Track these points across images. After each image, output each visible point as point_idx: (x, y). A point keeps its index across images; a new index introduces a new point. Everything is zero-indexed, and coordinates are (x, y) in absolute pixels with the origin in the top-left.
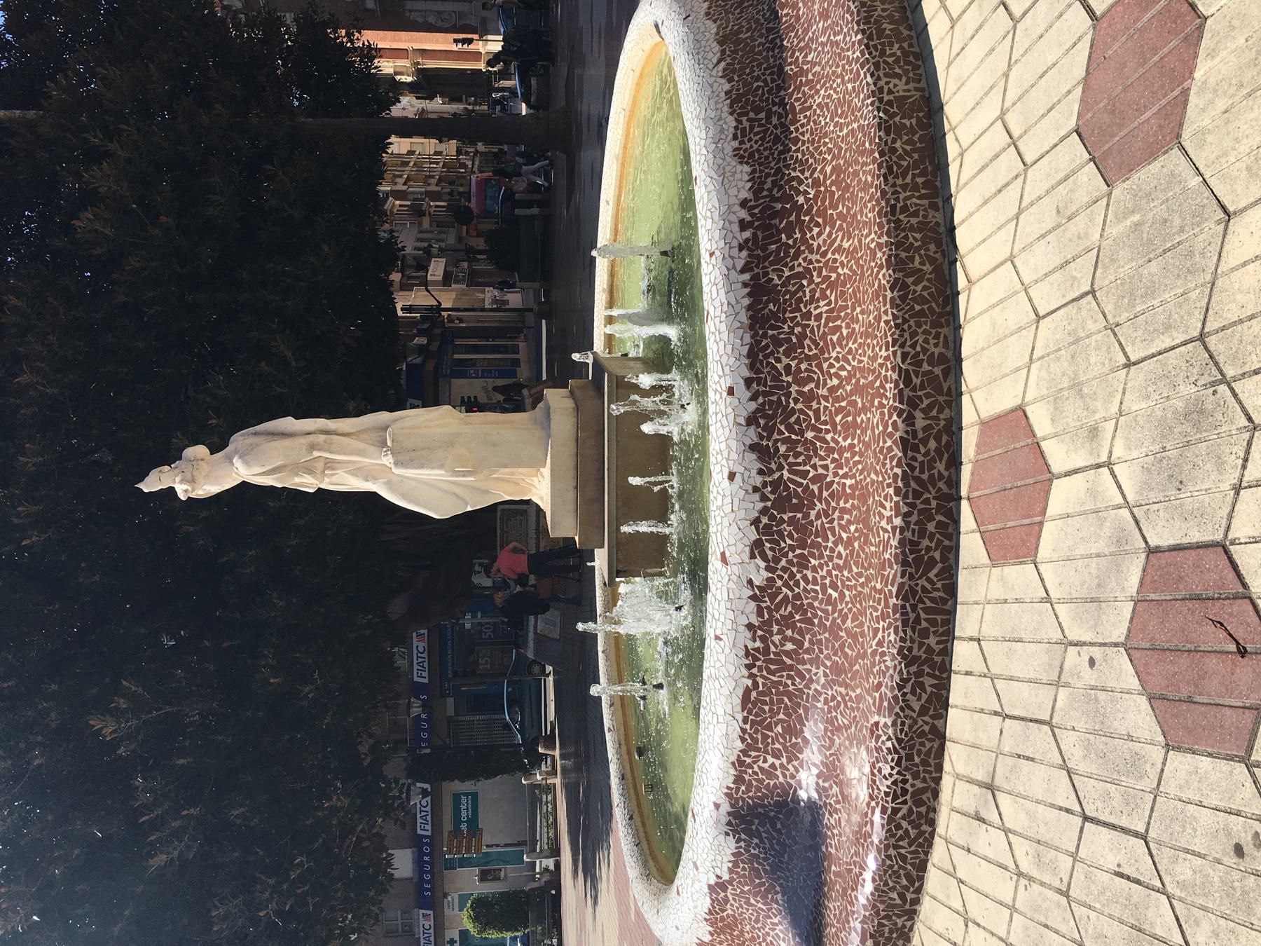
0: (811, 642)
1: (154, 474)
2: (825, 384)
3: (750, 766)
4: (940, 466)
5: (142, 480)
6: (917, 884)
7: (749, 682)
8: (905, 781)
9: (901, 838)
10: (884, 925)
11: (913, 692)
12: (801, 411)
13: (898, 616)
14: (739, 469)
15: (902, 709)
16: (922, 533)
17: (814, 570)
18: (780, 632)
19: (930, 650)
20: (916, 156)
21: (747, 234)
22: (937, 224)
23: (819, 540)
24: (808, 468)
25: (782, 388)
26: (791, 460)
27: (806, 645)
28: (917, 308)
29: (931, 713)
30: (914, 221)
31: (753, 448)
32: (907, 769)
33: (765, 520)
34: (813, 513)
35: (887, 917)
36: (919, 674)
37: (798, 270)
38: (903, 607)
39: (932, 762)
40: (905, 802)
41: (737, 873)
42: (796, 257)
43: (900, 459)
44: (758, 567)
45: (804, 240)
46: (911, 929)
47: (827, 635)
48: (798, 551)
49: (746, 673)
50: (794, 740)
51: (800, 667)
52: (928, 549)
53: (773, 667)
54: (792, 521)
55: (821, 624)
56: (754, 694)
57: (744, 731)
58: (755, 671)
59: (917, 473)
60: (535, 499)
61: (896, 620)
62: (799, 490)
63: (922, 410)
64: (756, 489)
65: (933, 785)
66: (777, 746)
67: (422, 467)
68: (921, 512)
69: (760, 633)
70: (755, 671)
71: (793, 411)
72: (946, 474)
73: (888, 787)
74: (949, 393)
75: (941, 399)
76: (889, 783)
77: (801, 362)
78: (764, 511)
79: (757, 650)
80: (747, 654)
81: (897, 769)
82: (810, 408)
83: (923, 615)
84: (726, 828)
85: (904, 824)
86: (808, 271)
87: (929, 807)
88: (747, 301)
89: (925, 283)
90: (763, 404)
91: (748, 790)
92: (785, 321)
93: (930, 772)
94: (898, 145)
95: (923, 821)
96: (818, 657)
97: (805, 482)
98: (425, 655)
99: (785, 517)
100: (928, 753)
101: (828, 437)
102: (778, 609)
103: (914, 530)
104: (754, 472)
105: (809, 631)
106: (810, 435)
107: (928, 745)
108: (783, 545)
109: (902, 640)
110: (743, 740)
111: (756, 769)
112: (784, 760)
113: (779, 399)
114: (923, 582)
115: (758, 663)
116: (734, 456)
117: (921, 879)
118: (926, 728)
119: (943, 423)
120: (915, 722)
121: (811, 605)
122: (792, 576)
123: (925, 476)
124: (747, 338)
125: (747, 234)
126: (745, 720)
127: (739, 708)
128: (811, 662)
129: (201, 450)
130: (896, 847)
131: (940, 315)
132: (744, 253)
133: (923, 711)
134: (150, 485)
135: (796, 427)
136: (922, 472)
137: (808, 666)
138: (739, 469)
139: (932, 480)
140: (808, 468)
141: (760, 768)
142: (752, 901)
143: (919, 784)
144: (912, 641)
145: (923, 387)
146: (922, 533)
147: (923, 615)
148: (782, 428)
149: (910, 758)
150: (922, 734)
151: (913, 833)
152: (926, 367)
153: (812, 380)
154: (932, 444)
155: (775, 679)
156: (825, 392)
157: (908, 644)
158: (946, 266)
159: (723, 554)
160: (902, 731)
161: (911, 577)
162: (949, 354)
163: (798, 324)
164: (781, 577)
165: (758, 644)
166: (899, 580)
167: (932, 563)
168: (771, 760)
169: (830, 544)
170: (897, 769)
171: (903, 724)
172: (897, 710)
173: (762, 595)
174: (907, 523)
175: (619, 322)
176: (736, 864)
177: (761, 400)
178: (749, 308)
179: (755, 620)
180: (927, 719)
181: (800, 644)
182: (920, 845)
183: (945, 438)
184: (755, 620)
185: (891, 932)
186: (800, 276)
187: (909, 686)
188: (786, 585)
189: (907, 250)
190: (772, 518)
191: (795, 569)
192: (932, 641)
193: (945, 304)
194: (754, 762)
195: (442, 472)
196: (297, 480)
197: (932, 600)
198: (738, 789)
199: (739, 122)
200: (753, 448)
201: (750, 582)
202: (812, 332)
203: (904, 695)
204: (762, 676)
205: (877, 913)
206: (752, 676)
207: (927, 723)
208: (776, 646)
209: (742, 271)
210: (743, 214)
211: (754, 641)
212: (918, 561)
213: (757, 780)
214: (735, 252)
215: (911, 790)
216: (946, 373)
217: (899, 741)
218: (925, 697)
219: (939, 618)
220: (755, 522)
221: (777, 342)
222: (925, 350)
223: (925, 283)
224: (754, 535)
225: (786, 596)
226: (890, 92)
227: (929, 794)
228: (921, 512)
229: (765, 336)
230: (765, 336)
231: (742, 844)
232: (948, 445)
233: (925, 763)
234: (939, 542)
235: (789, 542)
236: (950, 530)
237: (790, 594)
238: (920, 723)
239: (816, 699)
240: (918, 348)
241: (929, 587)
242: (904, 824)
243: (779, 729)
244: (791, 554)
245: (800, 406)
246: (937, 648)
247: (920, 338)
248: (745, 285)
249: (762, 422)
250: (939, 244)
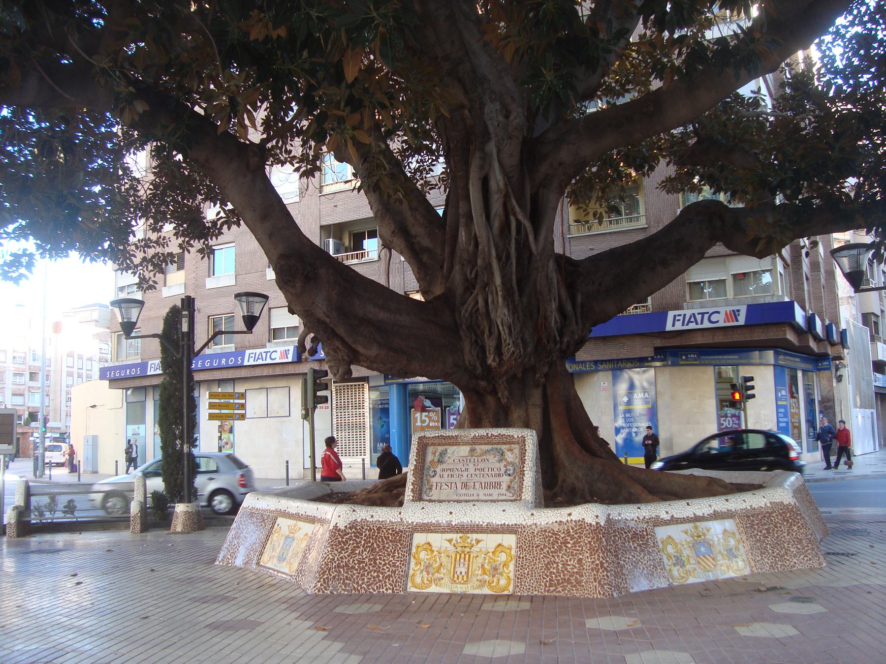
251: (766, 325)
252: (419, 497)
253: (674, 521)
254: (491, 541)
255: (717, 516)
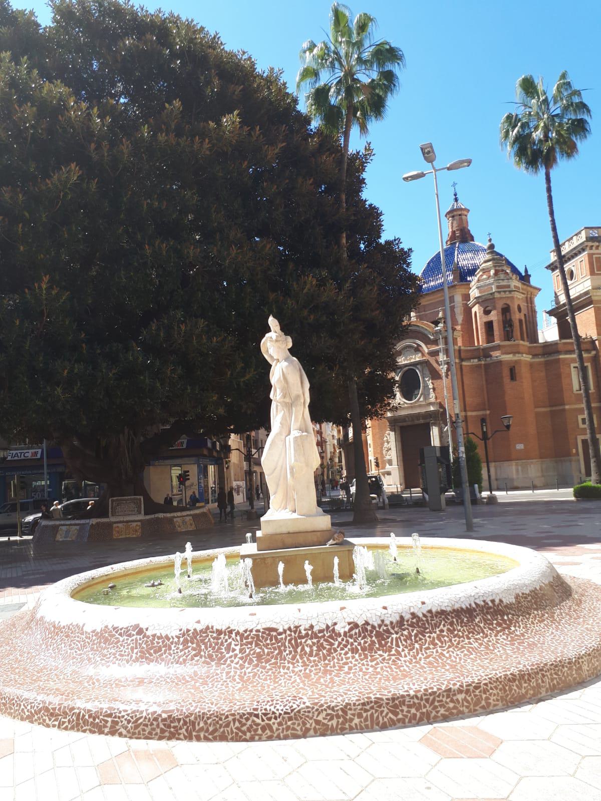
0: (314, 661)
1: (276, 322)
2: (444, 650)
3: (230, 637)
4: (442, 711)
5: (274, 317)
6: (210, 737)
7: (281, 630)
8: (276, 718)
9: (240, 722)
10: (179, 723)
11: (328, 715)
12: (426, 640)
13: (366, 700)
14: (390, 611)
15: (317, 710)
16: (409, 706)
17: (353, 657)
18: (314, 644)
19: (351, 720)
20: (563, 678)
21: (490, 604)
22: (541, 693)
23: (369, 658)
24: (401, 647)
25: (433, 629)
26: (402, 638)
27: (312, 659)
28: (507, 688)
29: (317, 727)
30: (540, 681)
31: (402, 617)
32: (283, 718)
33: (369, 628)
34: (380, 652)
35: (185, 723)
36: (338, 716)
37: (485, 630)
38: (371, 702)
39: (289, 732)
40: (263, 720)
41: (154, 639)
42: (490, 629)
43: (441, 689)
44: (344, 627)
45: (498, 632)
46: (178, 739)
47: (322, 668)
48: (359, 647)
49: (286, 627)
50: (254, 659)
51: (298, 657)
52: (402, 711)
53: (293, 642)
54: (373, 642)
55: (326, 665)
56: (274, 634)
57: (251, 631)
58: (288, 632)
59: (437, 699)
60: (269, 512)
61: (363, 699)
62: (389, 644)
63: (465, 697)
64: (383, 621)
65: (275, 735)
66: (248, 651)
67: (295, 450)
68: (419, 704)
69: (310, 632)
70: (288, 632)
71: (424, 636)
72: (439, 715)
73: (270, 710)
74: (475, 710)
75: (472, 707)
76: (273, 709)
77: (448, 637)
78: (373, 627)
79: (300, 632)
80: (297, 627)
81: (282, 713)
82: (429, 644)
83: (369, 713)
84: (185, 629)
85: (249, 723)
86: (487, 636)
87: (261, 735)
88: (464, 607)
89: (517, 690)
90: (423, 621)
91: (214, 638)
92: (462, 627)
93: (283, 732)
94: (566, 669)
95: (253, 733)
96: (308, 665)
97: (394, 646)
98: (23, 457)
99: (374, 638)
100: (294, 729)
101: (420, 655)
102: (326, 641)
103: (410, 701)
104: (391, 619)
105: (320, 658)
106: (417, 646)
107: (298, 728)
108: (360, 639)
109: (354, 704)
110: (246, 631)
111: (229, 641)
112: (240, 655)
113: (427, 628)
114: (386, 710)
115: (293, 634)
116: (395, 608)
117: (215, 739)
118: (308, 726)
119: (461, 709)
120: (311, 719)
121: (334, 658)
122: (345, 646)
123: (436, 704)
124: (449, 609)
125: (490, 604)
126: (258, 631)
127: (264, 626)
128: (304, 662)
129: (290, 345)
130: (234, 720)
131: (506, 700)
132: (482, 603)
133: (318, 722)
134: (272, 322)
135: (418, 639)
136: (439, 701)
137: (300, 661)
138: (390, 611)
139: (436, 707)
140: (401, 647)
141: (230, 643)
142: (135, 651)
143: (275, 727)
144: (355, 710)
145: (475, 696)
146: (409, 706)
147: (369, 713)
148: (415, 632)
149: (290, 719)
150: (304, 724)
151: (244, 728)
152: (484, 696)
153: (442, 644)
154: (451, 705)
155: (287, 644)
156: (440, 651)
157: (353, 708)
158: (526, 700)
159: (344, 608)
160: (305, 712)
161: (387, 704)
162: (491, 708)
163: (463, 633)
164: (343, 640)
165: (304, 632)
166: (384, 698)
167: (396, 714)
168: (238, 648)
169: (370, 664)
170: (282, 713)
171: (309, 712)
172: (316, 707)
173: (331, 632)
174: (412, 698)
175: (366, 551)
176: (160, 638)
177: (424, 619)
178: (462, 608)
179: (316, 629)
180: (314, 725)
181: (311, 655)
182: (237, 734)
183: (455, 711)
184: (316, 629)
185: (174, 727)
186: (483, 632)
187: (329, 712)
188: (340, 644)
189: (529, 680)
190: (371, 632)
191: (349, 646)
192: (356, 721)
193: (512, 703)
194: (233, 639)
195: (293, 461)
196: (278, 391)
197: (378, 717)
198: (213, 632)
199: (529, 595)
200: (402, 617)
201: (335, 624)
202: (463, 641)
203: (325, 710)
204: (286, 637)
205: (187, 716)
206: (285, 631)
207: (311, 725)
208: (305, 642)
209: (476, 603)
210: (497, 602)
211: (305, 630)
212: (396, 706)
213: (222, 642)
214: (482, 599)
215: (271, 723)
216: (483, 707)
217: (299, 711)
218: (326, 722)
219: (369, 723)
220: (367, 623)
221: (452, 624)
222: (490, 695)
223: (517, 690)
224: (360, 622)
225: (333, 644)
226: (583, 662)
227: (269, 734)
228: (419, 704)
229: (452, 618)
230: (452, 618)
231: (176, 640)
232: (452, 714)
233: (288, 728)
234: (406, 716)
235: (362, 642)
236: (413, 721)
237: (336, 646)
238: (311, 721)
239: (284, 668)
240: (491, 691)
241: (384, 714)
242: (249, 723)
243: (258, 650)
244: (356, 644)
245: (428, 639)
246: (353, 724)
247: (495, 692)
248: (470, 605)
249: (414, 620)
250: (534, 695)
251: (125, 575)
252: (112, 515)
253: (178, 517)
254: (134, 524)
255: (188, 515)
